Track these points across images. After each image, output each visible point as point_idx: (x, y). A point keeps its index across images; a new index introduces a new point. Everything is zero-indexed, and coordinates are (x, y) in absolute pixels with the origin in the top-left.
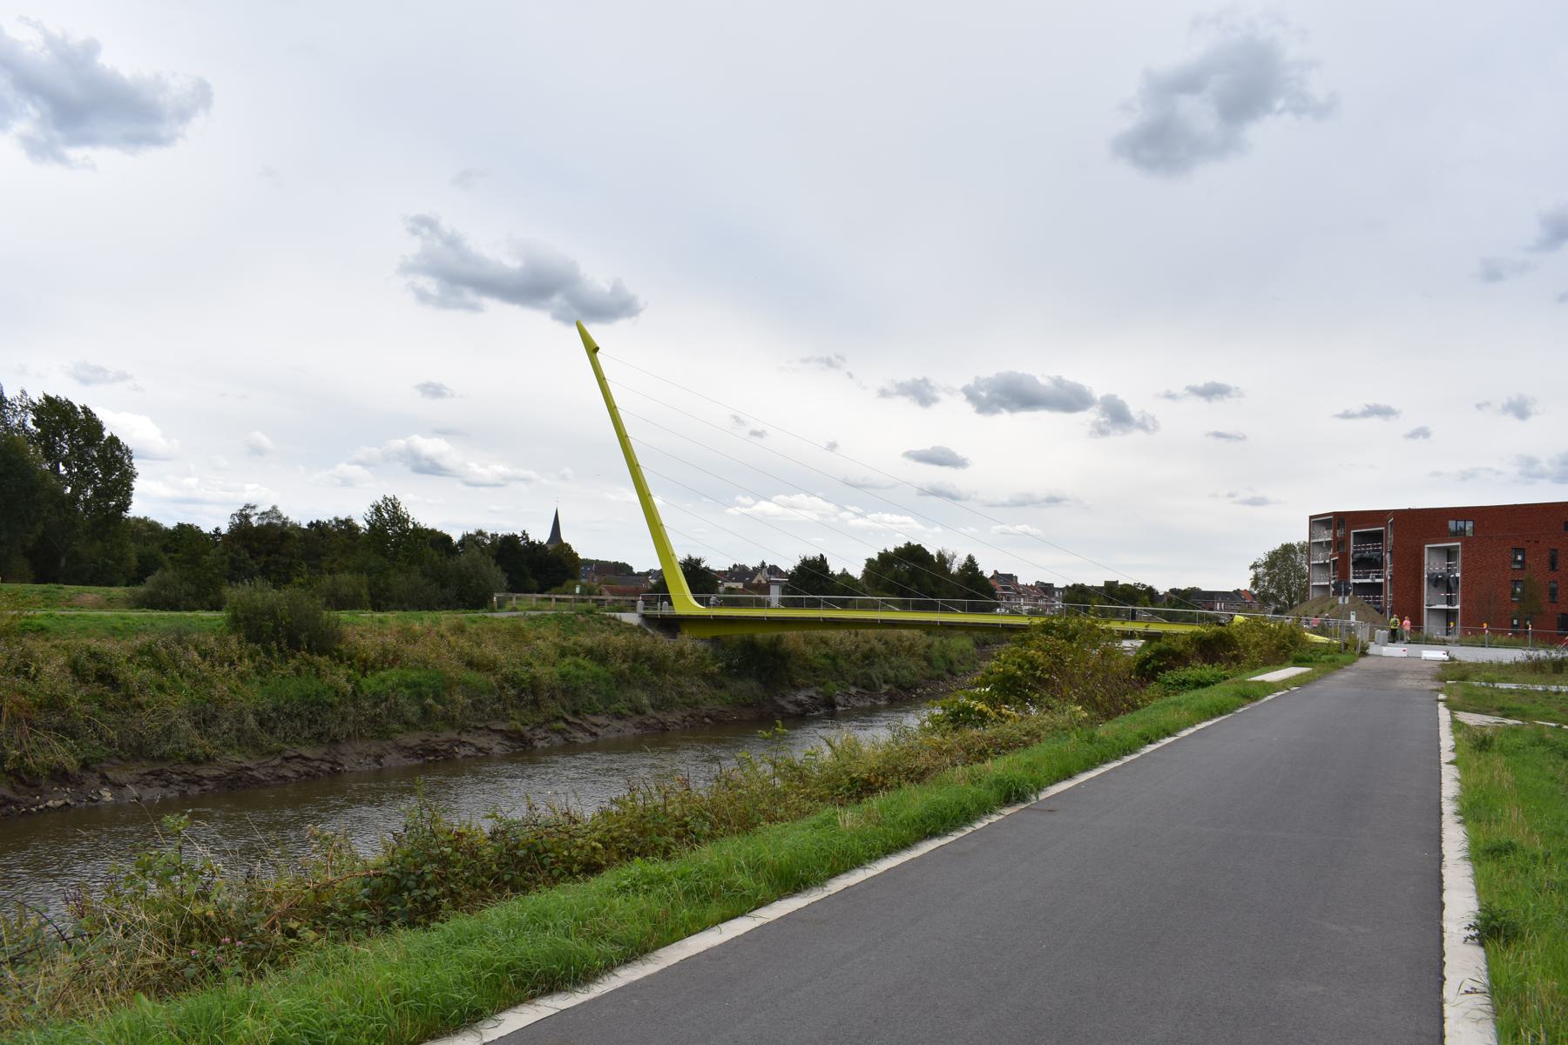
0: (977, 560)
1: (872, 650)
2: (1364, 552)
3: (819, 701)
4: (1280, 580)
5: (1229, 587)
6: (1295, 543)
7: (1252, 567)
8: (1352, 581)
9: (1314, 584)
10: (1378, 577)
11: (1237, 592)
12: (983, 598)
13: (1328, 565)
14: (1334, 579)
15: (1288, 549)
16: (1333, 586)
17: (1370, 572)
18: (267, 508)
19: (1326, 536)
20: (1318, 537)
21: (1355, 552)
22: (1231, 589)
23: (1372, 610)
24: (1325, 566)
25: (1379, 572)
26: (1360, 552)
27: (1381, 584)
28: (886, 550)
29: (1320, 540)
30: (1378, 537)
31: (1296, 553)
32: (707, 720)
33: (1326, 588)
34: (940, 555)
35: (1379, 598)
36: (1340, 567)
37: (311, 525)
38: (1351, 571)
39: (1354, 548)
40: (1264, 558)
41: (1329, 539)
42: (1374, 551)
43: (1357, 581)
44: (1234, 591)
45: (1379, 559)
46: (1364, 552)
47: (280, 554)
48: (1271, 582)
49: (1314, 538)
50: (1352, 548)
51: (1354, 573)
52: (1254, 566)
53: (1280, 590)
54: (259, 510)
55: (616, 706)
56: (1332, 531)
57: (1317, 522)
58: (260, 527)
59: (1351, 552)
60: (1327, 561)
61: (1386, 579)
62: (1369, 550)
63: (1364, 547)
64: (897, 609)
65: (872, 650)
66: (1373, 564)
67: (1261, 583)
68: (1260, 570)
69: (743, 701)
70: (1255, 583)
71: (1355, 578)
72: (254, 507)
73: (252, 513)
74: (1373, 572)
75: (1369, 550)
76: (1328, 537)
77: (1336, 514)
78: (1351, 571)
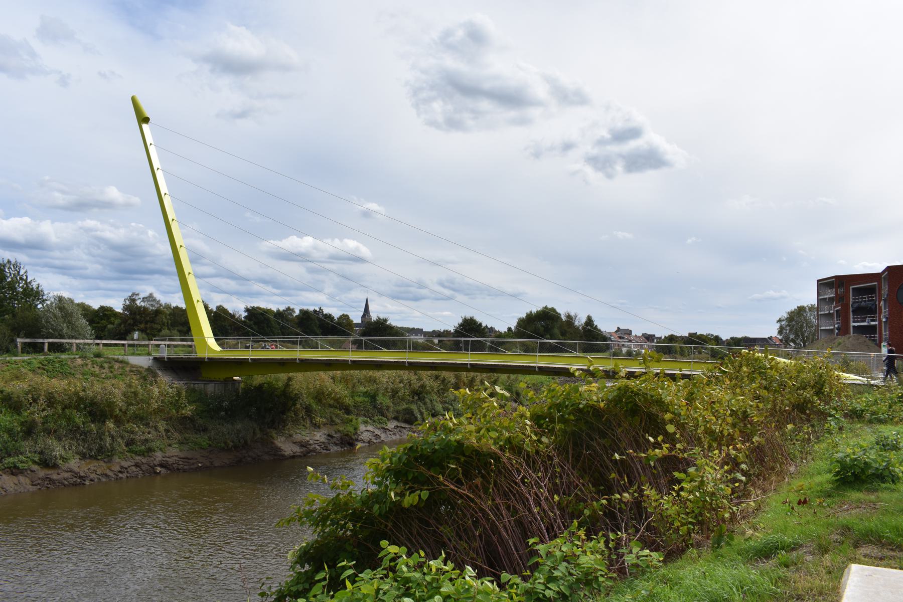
0: (594, 318)
1: (423, 386)
2: (861, 302)
3: (335, 440)
4: (796, 329)
5: (766, 336)
6: (805, 306)
7: (778, 321)
8: (852, 324)
9: (822, 328)
10: (872, 321)
11: (770, 338)
12: (556, 343)
13: (833, 314)
14: (837, 323)
15: (801, 310)
16: (837, 329)
17: (866, 317)
18: (146, 295)
19: (830, 294)
20: (824, 295)
21: (854, 303)
22: (766, 336)
23: (873, 345)
24: (830, 316)
25: (873, 317)
26: (857, 302)
27: (875, 326)
28: (531, 312)
29: (825, 297)
30: (871, 290)
31: (805, 311)
32: (159, 469)
33: (831, 331)
34: (569, 316)
35: (874, 337)
36: (843, 316)
37: (444, 331)
38: (851, 316)
39: (853, 299)
40: (786, 315)
41: (832, 295)
42: (869, 301)
43: (856, 324)
44: (769, 338)
45: (873, 307)
46: (861, 302)
47: (155, 323)
48: (791, 330)
49: (821, 296)
50: (851, 300)
51: (853, 318)
52: (780, 321)
53: (797, 336)
54: (142, 296)
55: (11, 460)
56: (834, 290)
57: (823, 284)
58: (141, 307)
59: (851, 303)
60: (832, 312)
61: (880, 321)
62: (864, 300)
63: (861, 298)
64: (384, 350)
65: (423, 386)
66: (871, 311)
67: (784, 331)
68: (783, 323)
69: (223, 445)
70: (780, 332)
71: (854, 322)
72: (138, 295)
73: (137, 298)
74: (869, 317)
75: (864, 300)
76: (831, 294)
77: (836, 277)
78: (851, 316)
